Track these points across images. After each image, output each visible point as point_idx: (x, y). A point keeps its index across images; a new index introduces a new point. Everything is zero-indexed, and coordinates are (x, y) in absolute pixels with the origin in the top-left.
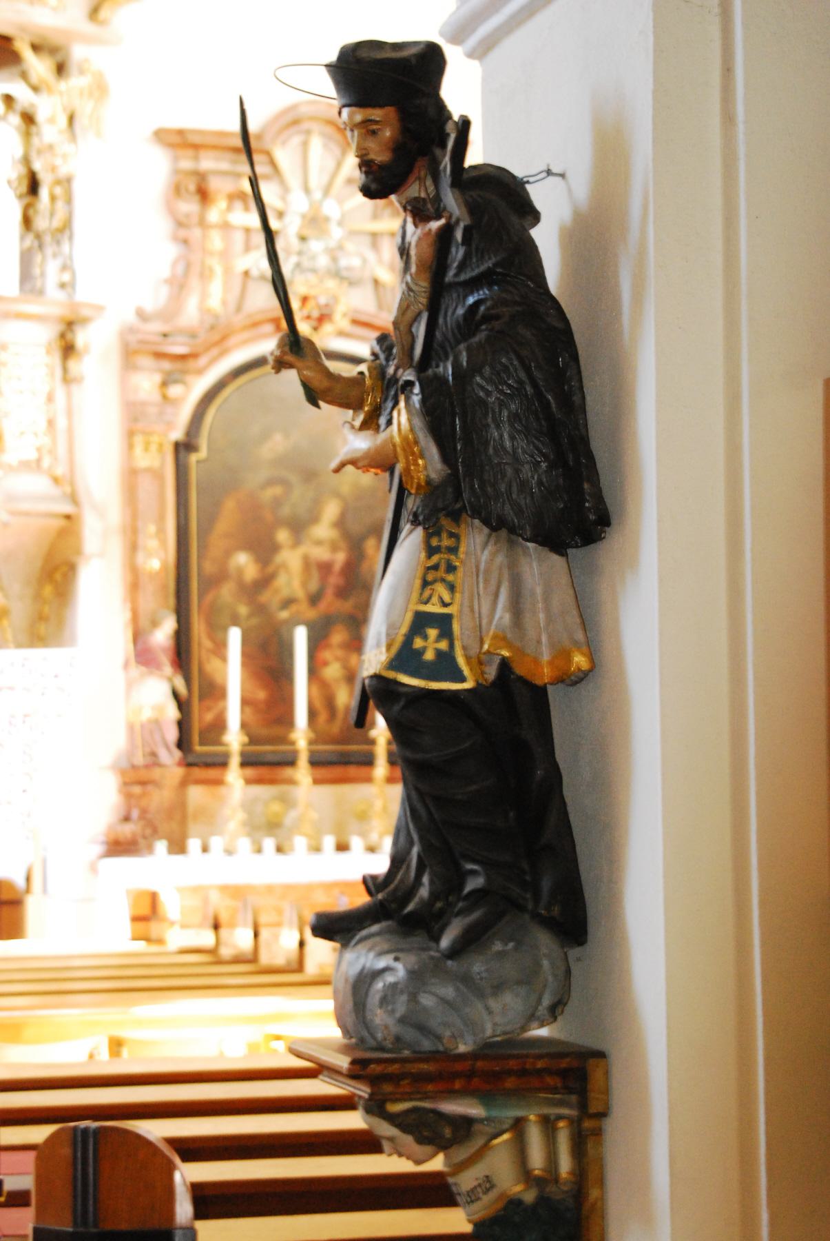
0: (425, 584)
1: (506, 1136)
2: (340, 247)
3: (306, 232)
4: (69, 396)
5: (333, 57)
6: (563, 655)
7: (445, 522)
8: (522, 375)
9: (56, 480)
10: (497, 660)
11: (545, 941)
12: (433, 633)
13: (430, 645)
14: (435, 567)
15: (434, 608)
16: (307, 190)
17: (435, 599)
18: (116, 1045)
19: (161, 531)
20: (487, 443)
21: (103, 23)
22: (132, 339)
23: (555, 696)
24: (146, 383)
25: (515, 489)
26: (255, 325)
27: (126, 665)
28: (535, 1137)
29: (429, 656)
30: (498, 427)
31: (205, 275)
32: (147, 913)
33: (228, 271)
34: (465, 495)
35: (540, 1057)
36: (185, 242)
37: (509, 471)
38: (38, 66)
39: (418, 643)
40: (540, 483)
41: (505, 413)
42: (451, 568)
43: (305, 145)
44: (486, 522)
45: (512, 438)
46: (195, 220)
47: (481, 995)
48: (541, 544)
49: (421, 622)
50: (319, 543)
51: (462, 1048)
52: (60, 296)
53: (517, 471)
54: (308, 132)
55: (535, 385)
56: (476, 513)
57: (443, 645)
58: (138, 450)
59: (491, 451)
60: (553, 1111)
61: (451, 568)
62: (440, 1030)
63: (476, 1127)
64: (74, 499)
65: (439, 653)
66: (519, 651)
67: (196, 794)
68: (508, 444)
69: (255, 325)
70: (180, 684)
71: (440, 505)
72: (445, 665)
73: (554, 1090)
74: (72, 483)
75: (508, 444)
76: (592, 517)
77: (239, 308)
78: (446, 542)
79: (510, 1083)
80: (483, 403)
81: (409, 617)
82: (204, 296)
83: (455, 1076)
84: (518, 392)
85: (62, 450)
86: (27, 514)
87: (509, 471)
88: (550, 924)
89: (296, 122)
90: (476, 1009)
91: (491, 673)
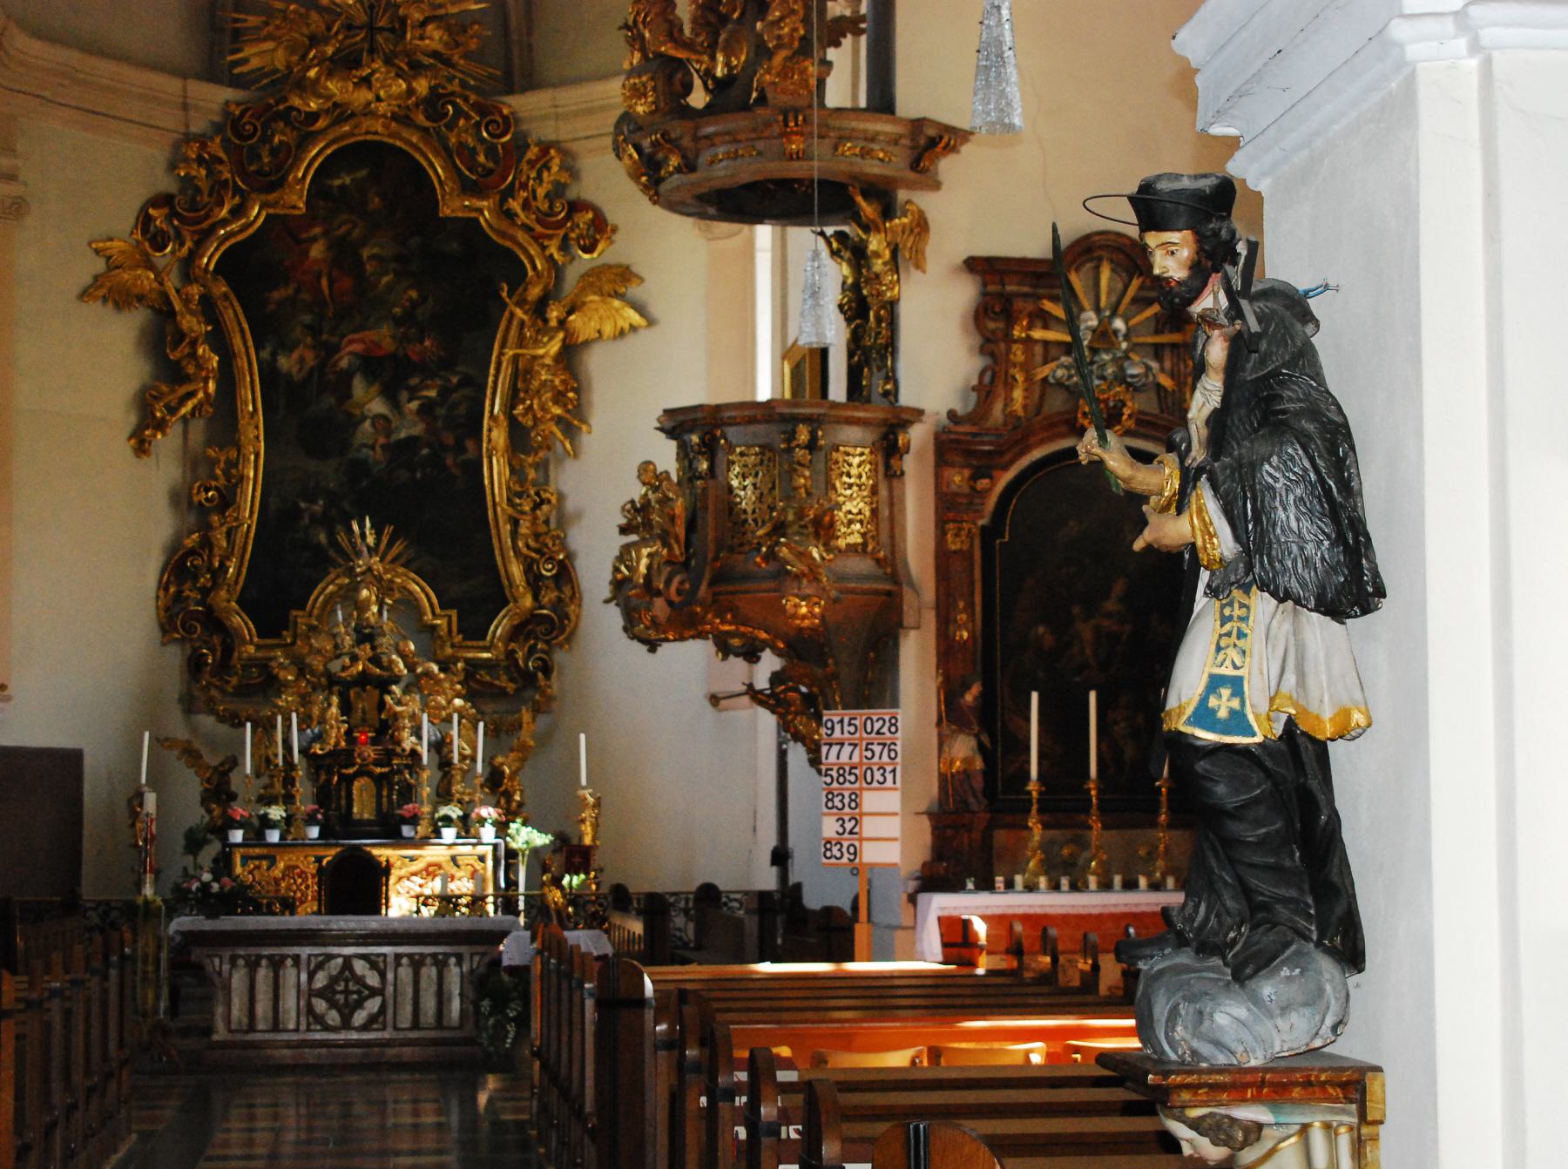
0: (1219, 649)
1: (1293, 1140)
2: (1127, 358)
3: (1096, 346)
4: (891, 490)
5: (1133, 189)
6: (1346, 714)
7: (1237, 594)
8: (1307, 464)
9: (878, 561)
10: (1284, 717)
11: (1326, 967)
12: (1225, 692)
13: (1223, 704)
14: (1229, 634)
15: (1228, 671)
16: (1098, 310)
17: (1228, 663)
18: (935, 1054)
19: (970, 605)
20: (1275, 524)
21: (924, 171)
22: (944, 437)
23: (1336, 750)
24: (957, 479)
25: (1300, 565)
26: (1052, 425)
27: (939, 723)
28: (1318, 1138)
29: (1223, 714)
30: (1285, 509)
31: (1010, 384)
32: (957, 937)
33: (1029, 379)
34: (1257, 570)
35: (1323, 1070)
36: (992, 355)
37: (1295, 548)
38: (868, 209)
39: (1213, 702)
40: (1323, 559)
41: (1291, 497)
42: (1241, 635)
43: (1097, 269)
44: (1274, 594)
45: (1298, 520)
46: (1000, 335)
47: (1271, 1016)
48: (1325, 614)
49: (1215, 683)
50: (1109, 615)
51: (1253, 1063)
52: (884, 403)
53: (1302, 549)
54: (1100, 259)
55: (1317, 472)
56: (1263, 587)
57: (1235, 704)
58: (949, 537)
59: (1278, 531)
60: (1335, 1119)
61: (1241, 635)
62: (1233, 1046)
63: (1266, 1132)
64: (894, 578)
65: (1232, 712)
66: (1304, 711)
67: (1001, 837)
68: (1294, 524)
69: (1052, 425)
70: (985, 738)
71: (1233, 578)
72: (1237, 721)
73: (1336, 1100)
74: (893, 566)
75: (1294, 524)
76: (1370, 589)
77: (1037, 414)
78: (1237, 612)
79: (1296, 1092)
80: (1271, 488)
81: (1205, 677)
82: (1009, 400)
83: (1247, 1086)
84: (1304, 477)
85: (884, 537)
86: (853, 591)
87: (1295, 548)
88: (1332, 952)
89: (1089, 250)
90: (1265, 1027)
91: (1279, 729)
